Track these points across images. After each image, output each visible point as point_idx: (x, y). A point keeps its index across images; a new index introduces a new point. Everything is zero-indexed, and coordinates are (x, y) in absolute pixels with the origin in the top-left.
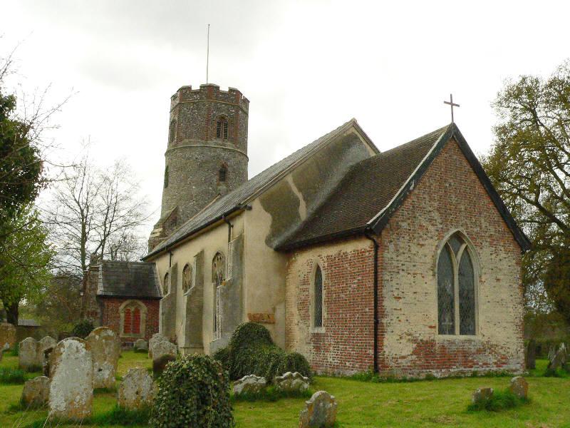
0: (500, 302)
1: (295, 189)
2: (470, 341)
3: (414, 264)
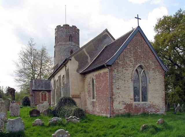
1: (86, 53)
2: (145, 104)
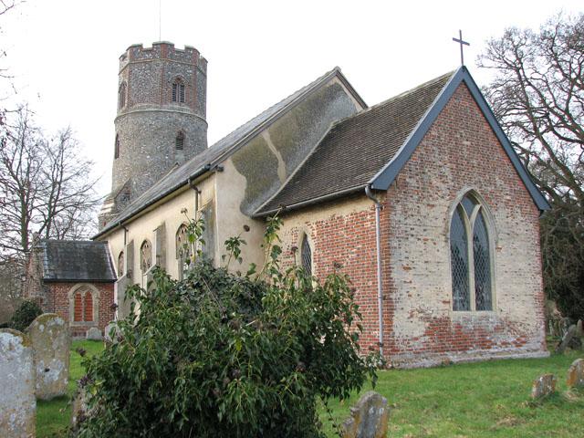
0: (518, 273)
2: (487, 318)
3: (425, 228)
